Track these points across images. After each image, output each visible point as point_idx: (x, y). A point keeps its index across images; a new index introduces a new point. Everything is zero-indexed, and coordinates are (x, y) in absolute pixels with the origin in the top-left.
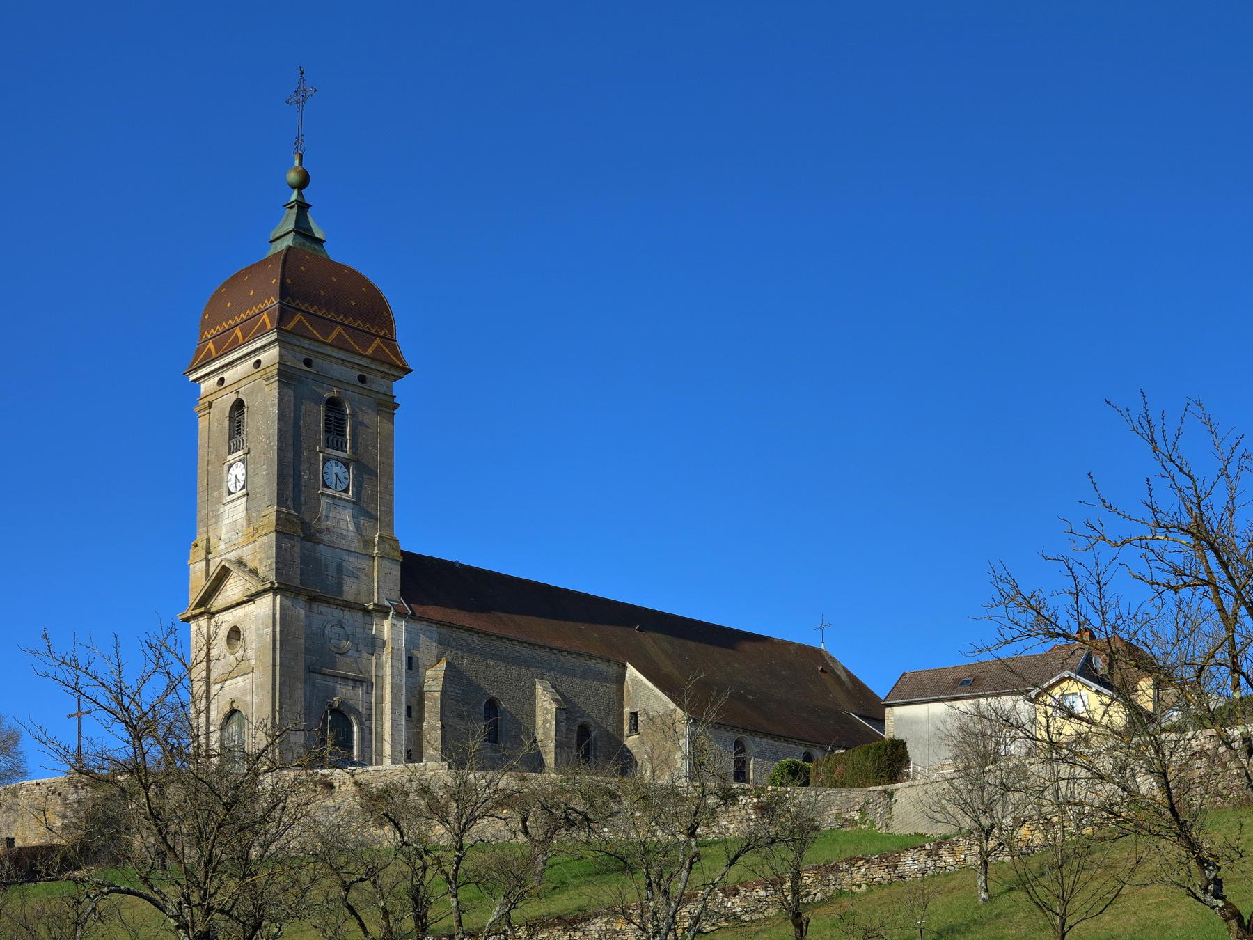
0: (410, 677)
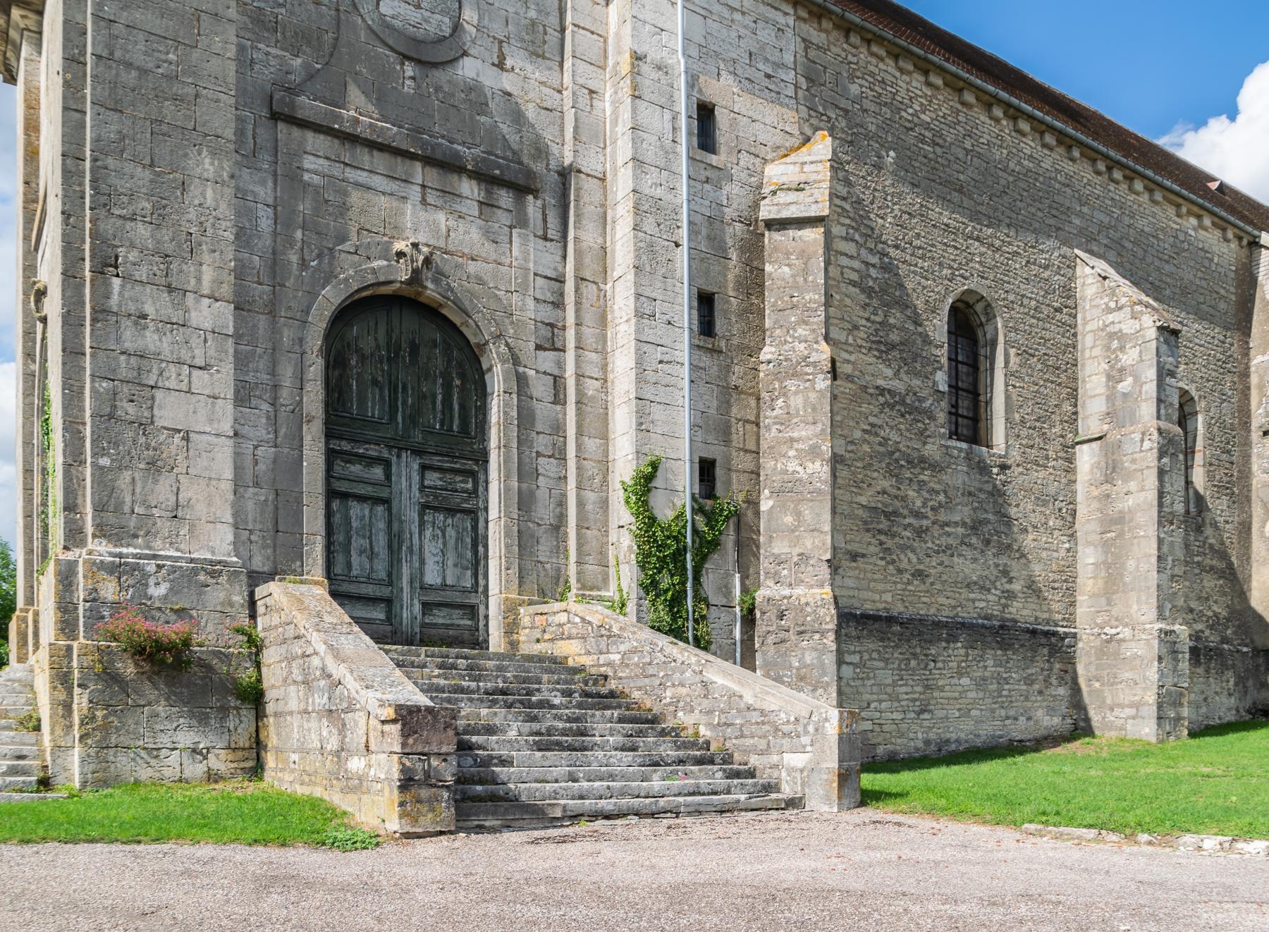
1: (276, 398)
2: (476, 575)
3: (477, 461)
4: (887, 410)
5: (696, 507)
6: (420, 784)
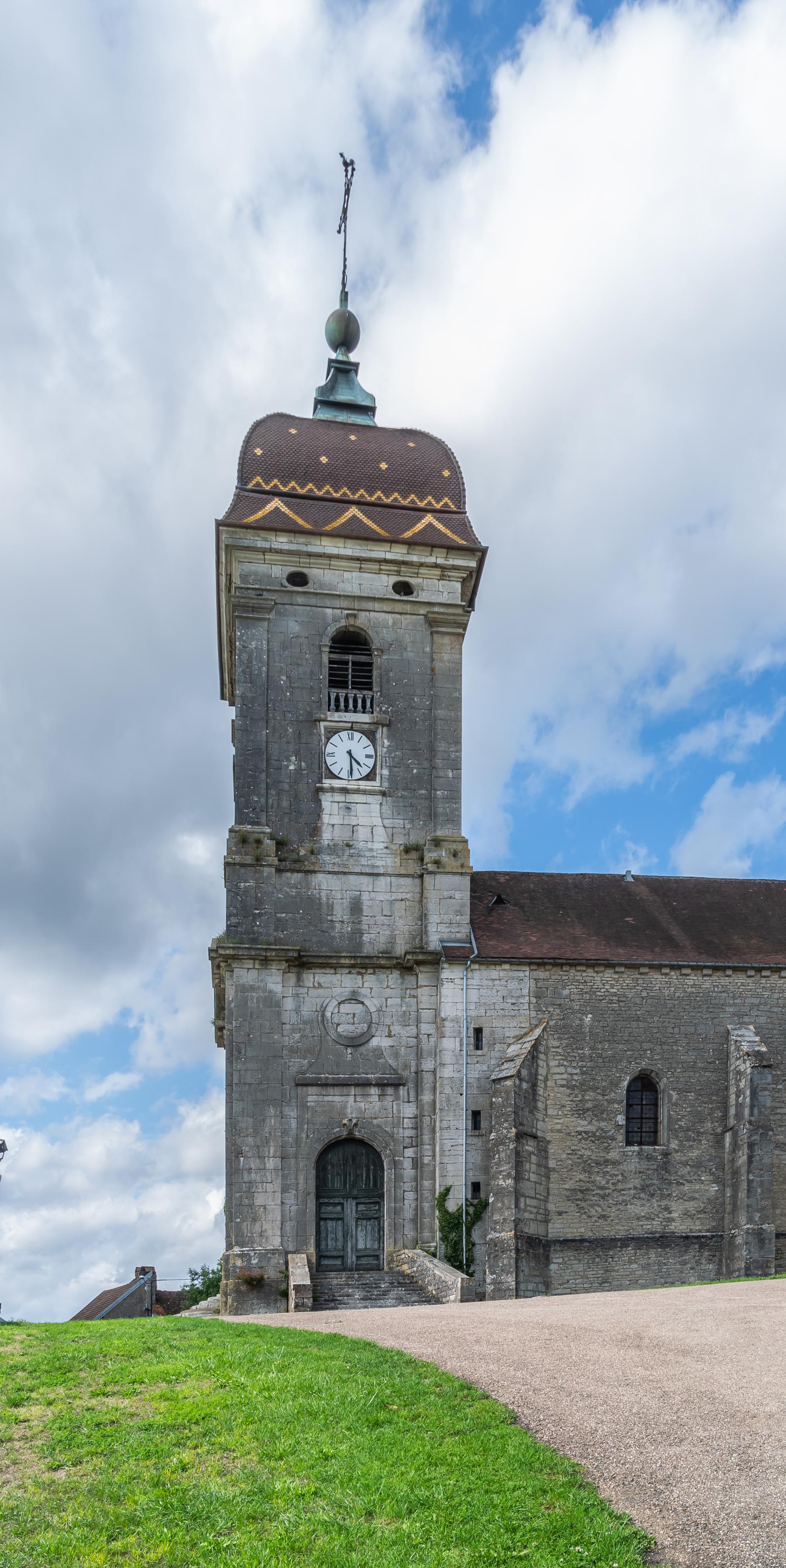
0: (478, 1062)
1: (297, 1188)
2: (379, 1243)
3: (380, 1198)
4: (583, 1141)
5: (468, 1203)
6: (300, 1306)
